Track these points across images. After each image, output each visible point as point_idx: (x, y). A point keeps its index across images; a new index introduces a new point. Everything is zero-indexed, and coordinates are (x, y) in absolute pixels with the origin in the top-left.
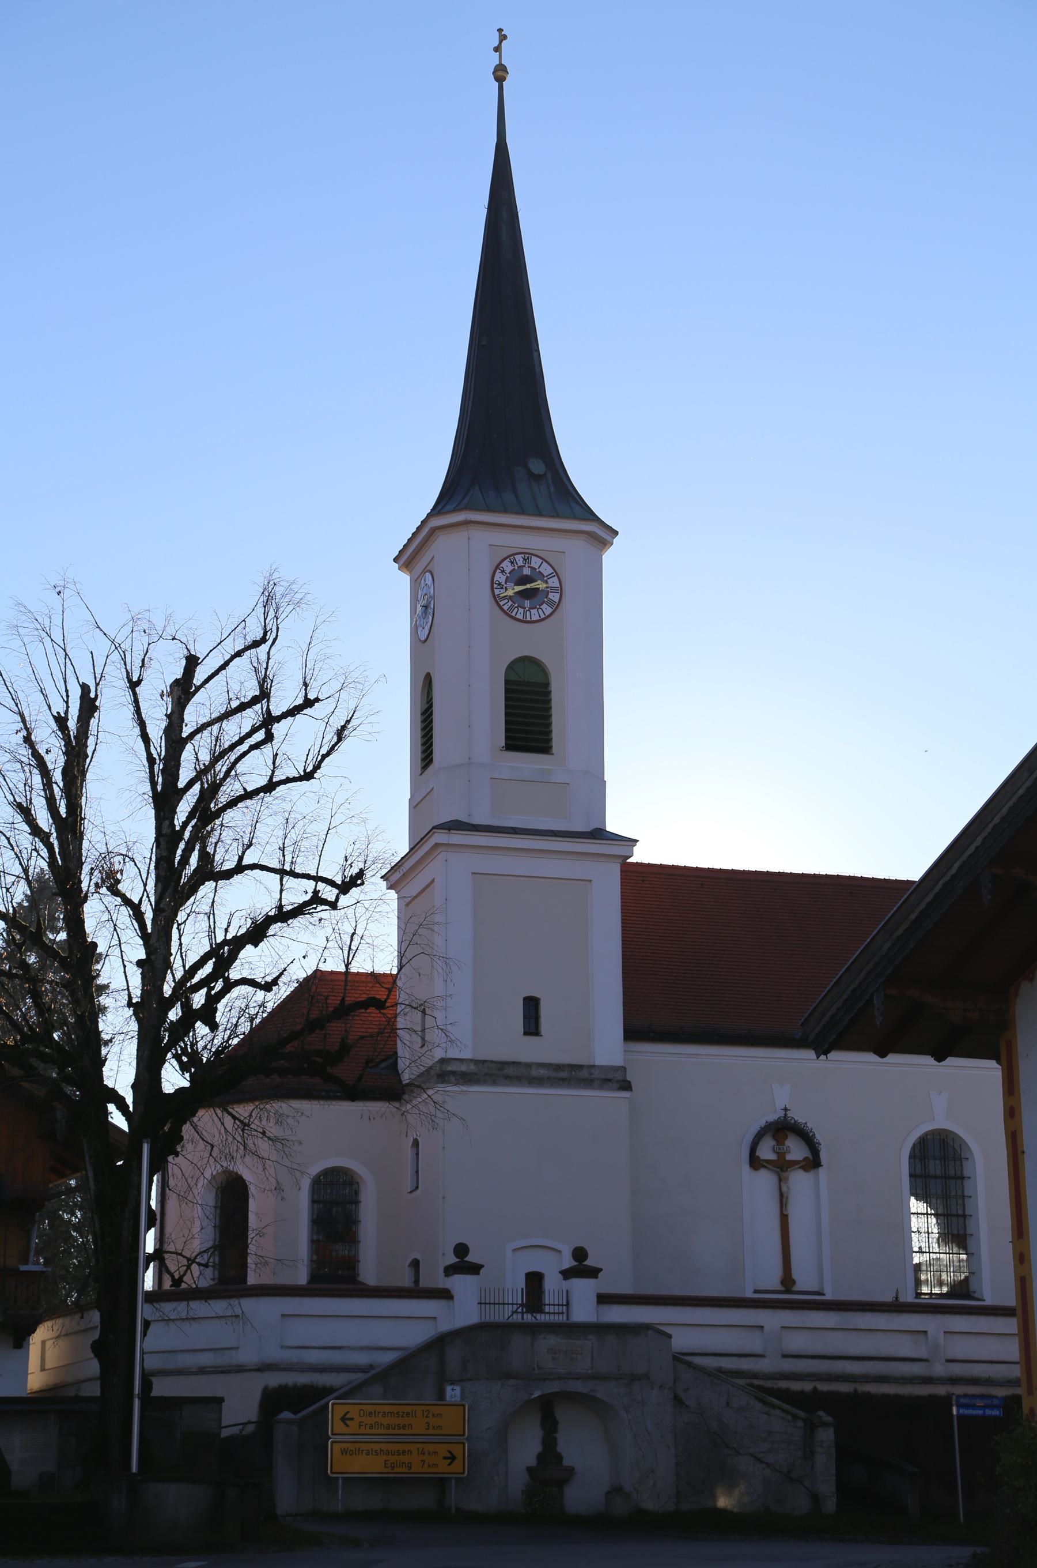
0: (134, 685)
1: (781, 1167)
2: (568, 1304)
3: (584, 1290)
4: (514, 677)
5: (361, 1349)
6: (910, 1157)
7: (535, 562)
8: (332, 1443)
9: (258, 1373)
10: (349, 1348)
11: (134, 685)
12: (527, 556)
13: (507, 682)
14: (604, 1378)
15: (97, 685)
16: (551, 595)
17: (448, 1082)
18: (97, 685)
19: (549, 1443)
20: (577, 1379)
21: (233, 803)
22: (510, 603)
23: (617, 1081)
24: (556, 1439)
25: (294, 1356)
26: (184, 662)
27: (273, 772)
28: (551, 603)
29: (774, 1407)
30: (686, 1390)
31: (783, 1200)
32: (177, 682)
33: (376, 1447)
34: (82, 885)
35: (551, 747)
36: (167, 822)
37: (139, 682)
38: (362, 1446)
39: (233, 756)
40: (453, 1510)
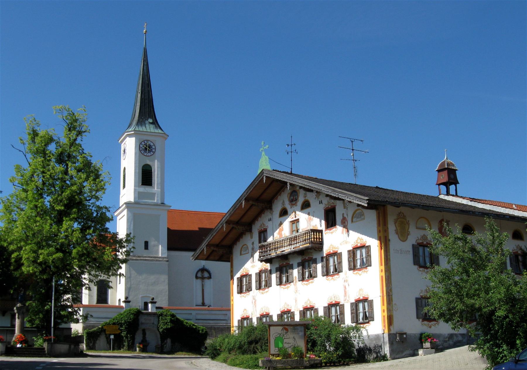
1: (203, 278)
28: (153, 152)
31: (203, 286)
34: (394, 228)
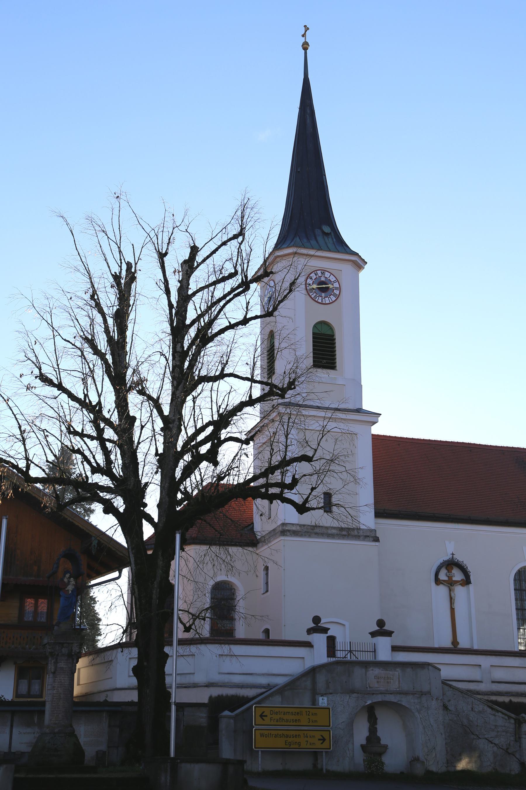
0: (162, 256)
1: (450, 584)
2: (375, 651)
3: (384, 644)
4: (317, 331)
5: (263, 675)
6: (515, 580)
7: (327, 275)
8: (255, 730)
9: (206, 688)
10: (256, 674)
11: (162, 256)
12: (323, 272)
13: (314, 334)
14: (406, 693)
15: (136, 264)
16: (335, 291)
17: (287, 535)
18: (136, 264)
19: (373, 730)
20: (391, 694)
21: (222, 331)
22: (315, 294)
23: (372, 537)
24: (376, 728)
25: (226, 679)
26: (189, 250)
27: (246, 314)
28: (335, 295)
29: (498, 711)
30: (449, 701)
31: (451, 600)
32: (185, 262)
33: (280, 732)
35: (336, 367)
36: (179, 344)
37: (166, 254)
38: (273, 732)
39: (222, 303)
40: (324, 771)
